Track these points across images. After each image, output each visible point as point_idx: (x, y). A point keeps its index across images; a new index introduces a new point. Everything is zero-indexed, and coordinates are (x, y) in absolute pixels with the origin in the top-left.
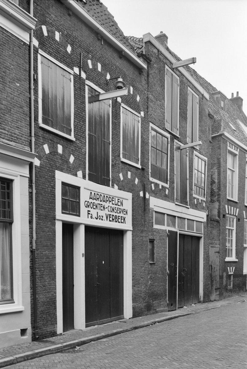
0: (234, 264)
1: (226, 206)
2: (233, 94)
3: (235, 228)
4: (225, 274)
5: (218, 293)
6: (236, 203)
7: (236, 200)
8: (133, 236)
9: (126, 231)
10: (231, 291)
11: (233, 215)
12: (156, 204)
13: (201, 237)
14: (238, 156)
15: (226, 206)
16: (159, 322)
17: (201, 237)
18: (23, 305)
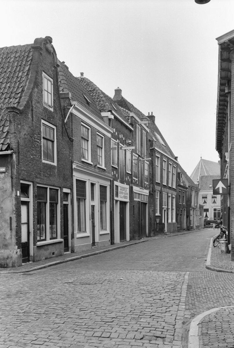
0: (159, 217)
1: (156, 186)
2: (149, 113)
3: (159, 197)
4: (155, 223)
5: (153, 233)
6: (159, 183)
7: (159, 182)
8: (130, 204)
9: (128, 202)
10: (158, 232)
11: (165, 192)
12: (136, 189)
13: (147, 203)
14: (160, 158)
15: (156, 186)
16: (141, 242)
17: (147, 203)
18: (90, 233)
